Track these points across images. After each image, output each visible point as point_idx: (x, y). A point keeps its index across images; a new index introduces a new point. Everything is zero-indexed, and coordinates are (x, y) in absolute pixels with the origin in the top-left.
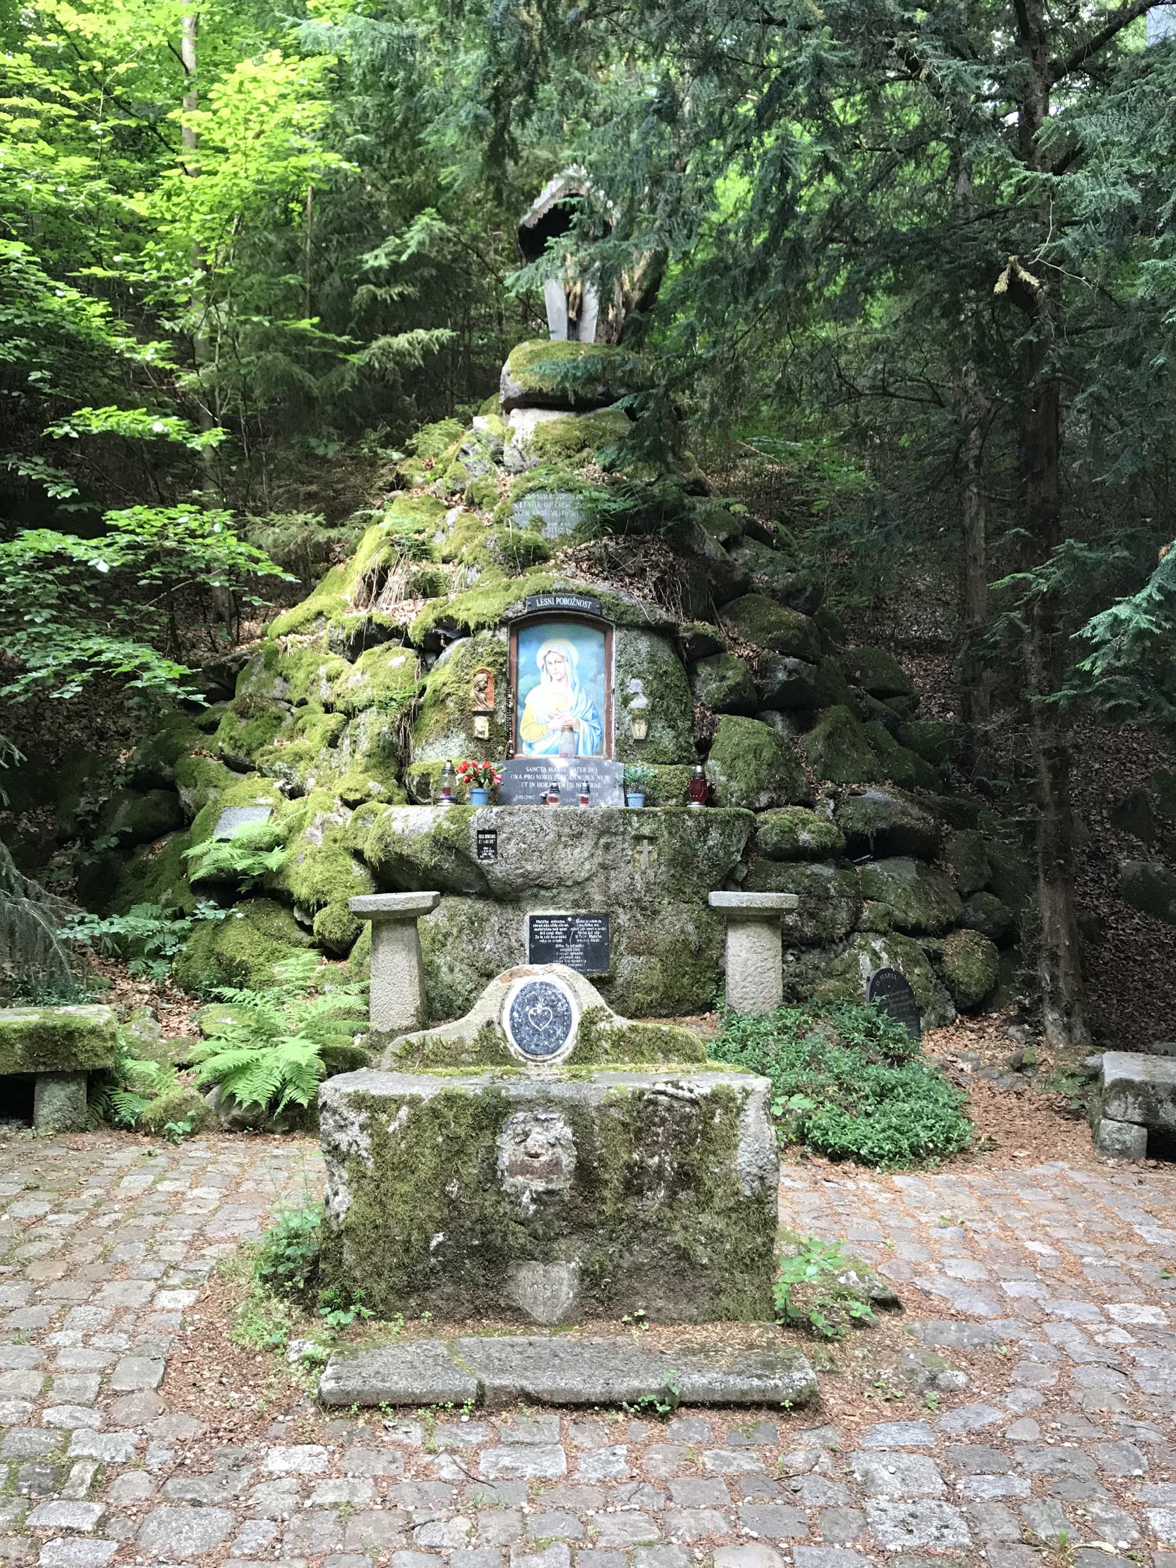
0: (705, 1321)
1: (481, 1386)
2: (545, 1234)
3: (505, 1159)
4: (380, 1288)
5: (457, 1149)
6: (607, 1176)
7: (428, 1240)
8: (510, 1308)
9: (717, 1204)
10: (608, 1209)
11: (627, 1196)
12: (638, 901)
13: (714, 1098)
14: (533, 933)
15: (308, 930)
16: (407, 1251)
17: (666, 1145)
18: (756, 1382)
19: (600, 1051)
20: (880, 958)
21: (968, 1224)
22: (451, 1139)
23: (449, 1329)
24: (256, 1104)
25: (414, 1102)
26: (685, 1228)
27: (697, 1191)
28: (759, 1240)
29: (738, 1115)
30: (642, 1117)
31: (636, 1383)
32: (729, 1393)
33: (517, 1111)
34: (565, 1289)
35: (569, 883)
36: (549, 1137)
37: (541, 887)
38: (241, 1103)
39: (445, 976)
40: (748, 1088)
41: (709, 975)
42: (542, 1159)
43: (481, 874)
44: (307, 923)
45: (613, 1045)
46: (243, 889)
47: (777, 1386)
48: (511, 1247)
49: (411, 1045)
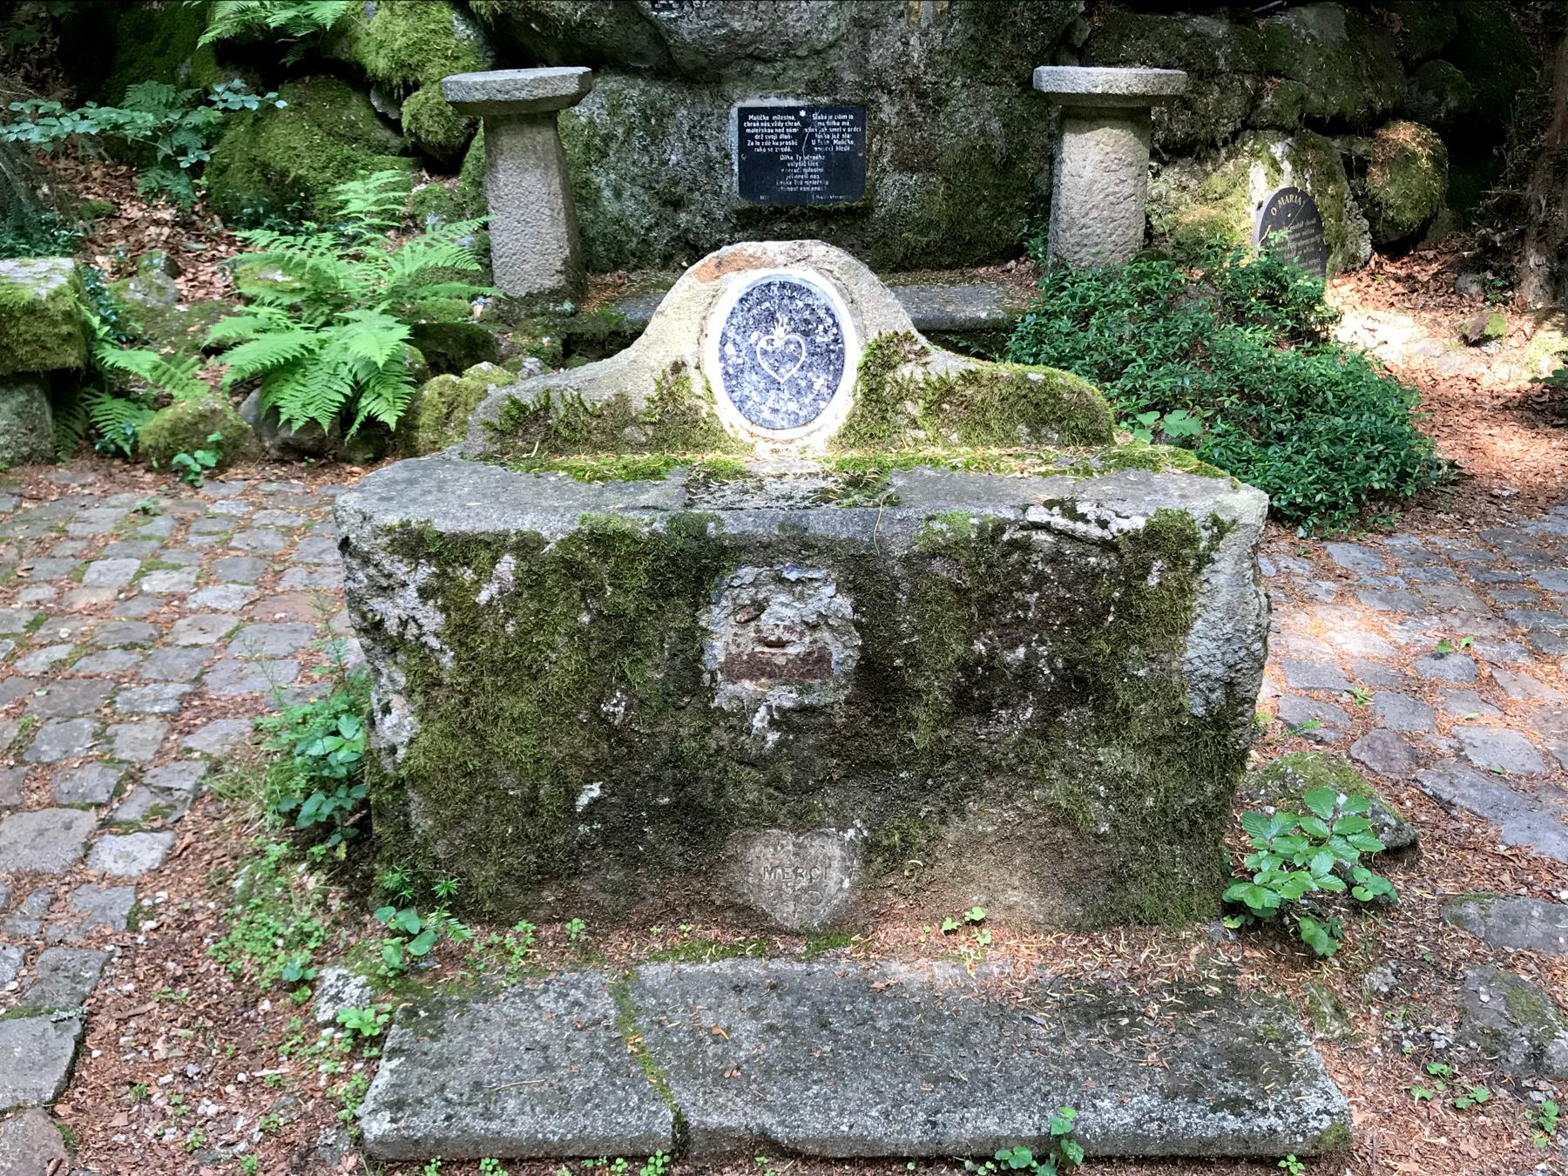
0: (1095, 927)
1: (681, 1124)
2: (796, 782)
3: (717, 651)
4: (485, 874)
5: (620, 638)
6: (920, 683)
7: (572, 795)
8: (731, 906)
9: (1137, 730)
10: (921, 738)
11: (956, 715)
12: (913, 82)
13: (1152, 539)
14: (743, 136)
15: (395, 126)
16: (531, 814)
17: (1042, 625)
18: (1232, 1123)
19: (901, 420)
20: (1279, 171)
21: (1476, 646)
22: (608, 618)
23: (619, 944)
24: (313, 423)
25: (527, 546)
26: (1069, 772)
27: (1097, 708)
28: (1210, 789)
29: (1198, 570)
30: (993, 570)
31: (990, 1125)
32: (1176, 1143)
33: (739, 565)
34: (835, 874)
35: (802, 52)
36: (804, 614)
37: (757, 58)
38: (289, 421)
39: (609, 205)
40: (1225, 518)
41: (1018, 202)
42: (791, 650)
43: (659, 36)
44: (393, 116)
45: (928, 411)
46: (289, 60)
47: (1272, 1131)
48: (732, 808)
49: (522, 408)
